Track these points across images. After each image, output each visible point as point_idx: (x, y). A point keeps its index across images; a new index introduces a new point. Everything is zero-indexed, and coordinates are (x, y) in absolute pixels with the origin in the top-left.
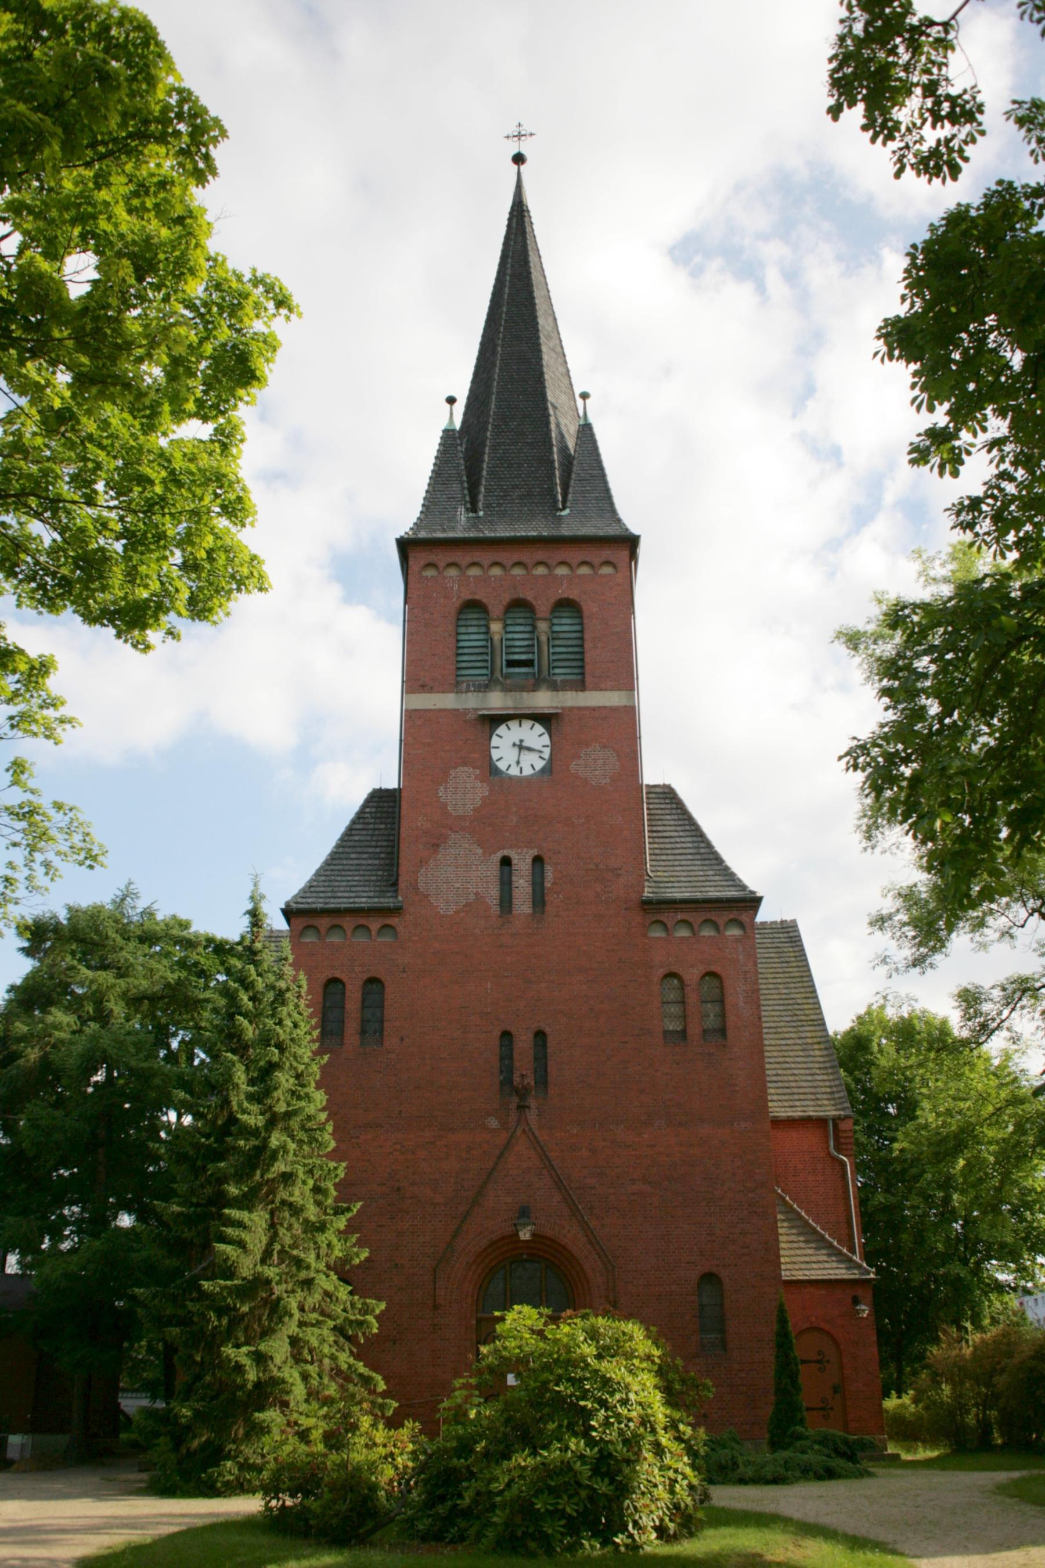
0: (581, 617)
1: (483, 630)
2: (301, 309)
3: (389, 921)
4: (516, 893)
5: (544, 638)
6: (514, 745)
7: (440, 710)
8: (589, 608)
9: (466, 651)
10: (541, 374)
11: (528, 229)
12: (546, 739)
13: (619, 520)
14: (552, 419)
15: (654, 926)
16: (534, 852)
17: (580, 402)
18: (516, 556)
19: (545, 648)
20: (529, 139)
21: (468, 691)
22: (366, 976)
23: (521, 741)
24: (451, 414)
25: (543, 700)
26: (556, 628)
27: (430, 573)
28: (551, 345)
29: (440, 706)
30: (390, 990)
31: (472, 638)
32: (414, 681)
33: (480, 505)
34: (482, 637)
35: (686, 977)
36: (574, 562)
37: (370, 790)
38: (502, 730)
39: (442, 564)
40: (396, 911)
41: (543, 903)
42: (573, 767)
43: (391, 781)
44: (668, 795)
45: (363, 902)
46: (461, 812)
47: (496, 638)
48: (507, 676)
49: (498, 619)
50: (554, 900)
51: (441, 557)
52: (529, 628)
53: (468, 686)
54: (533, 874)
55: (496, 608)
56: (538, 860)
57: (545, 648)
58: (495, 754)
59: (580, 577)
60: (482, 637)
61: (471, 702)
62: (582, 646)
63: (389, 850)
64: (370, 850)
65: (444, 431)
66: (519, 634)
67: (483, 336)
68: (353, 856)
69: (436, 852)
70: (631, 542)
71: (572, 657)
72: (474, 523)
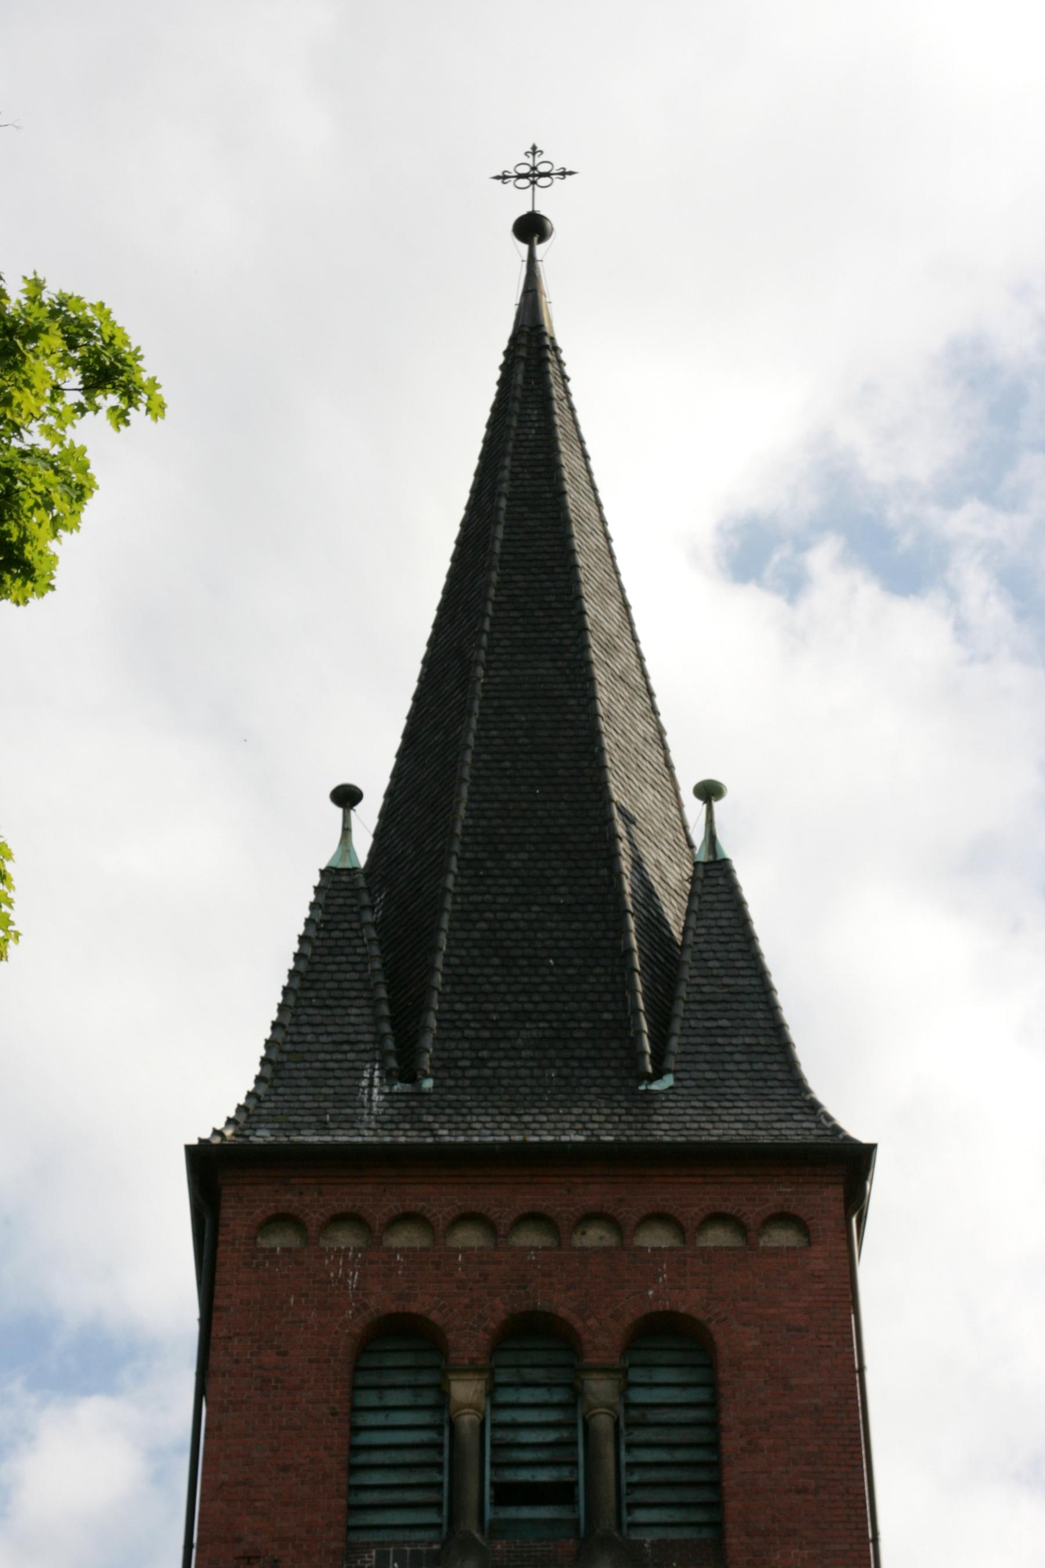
0: (711, 1366)
1: (429, 1398)
2: (165, 393)
5: (603, 1422)
9: (378, 1457)
10: (595, 735)
11: (556, 391)
13: (814, 1107)
14: (623, 846)
17: (694, 810)
19: (609, 1450)
20: (557, 181)
24: (346, 830)
26: (639, 1396)
27: (279, 1241)
28: (617, 666)
31: (397, 1422)
33: (426, 1062)
47: (467, 1420)
48: (498, 1530)
49: (473, 1369)
52: (558, 1396)
55: (468, 1341)
59: (709, 1255)
62: (714, 1446)
65: (325, 873)
66: (533, 1412)
67: (432, 643)
70: (852, 1163)
72: (409, 1108)
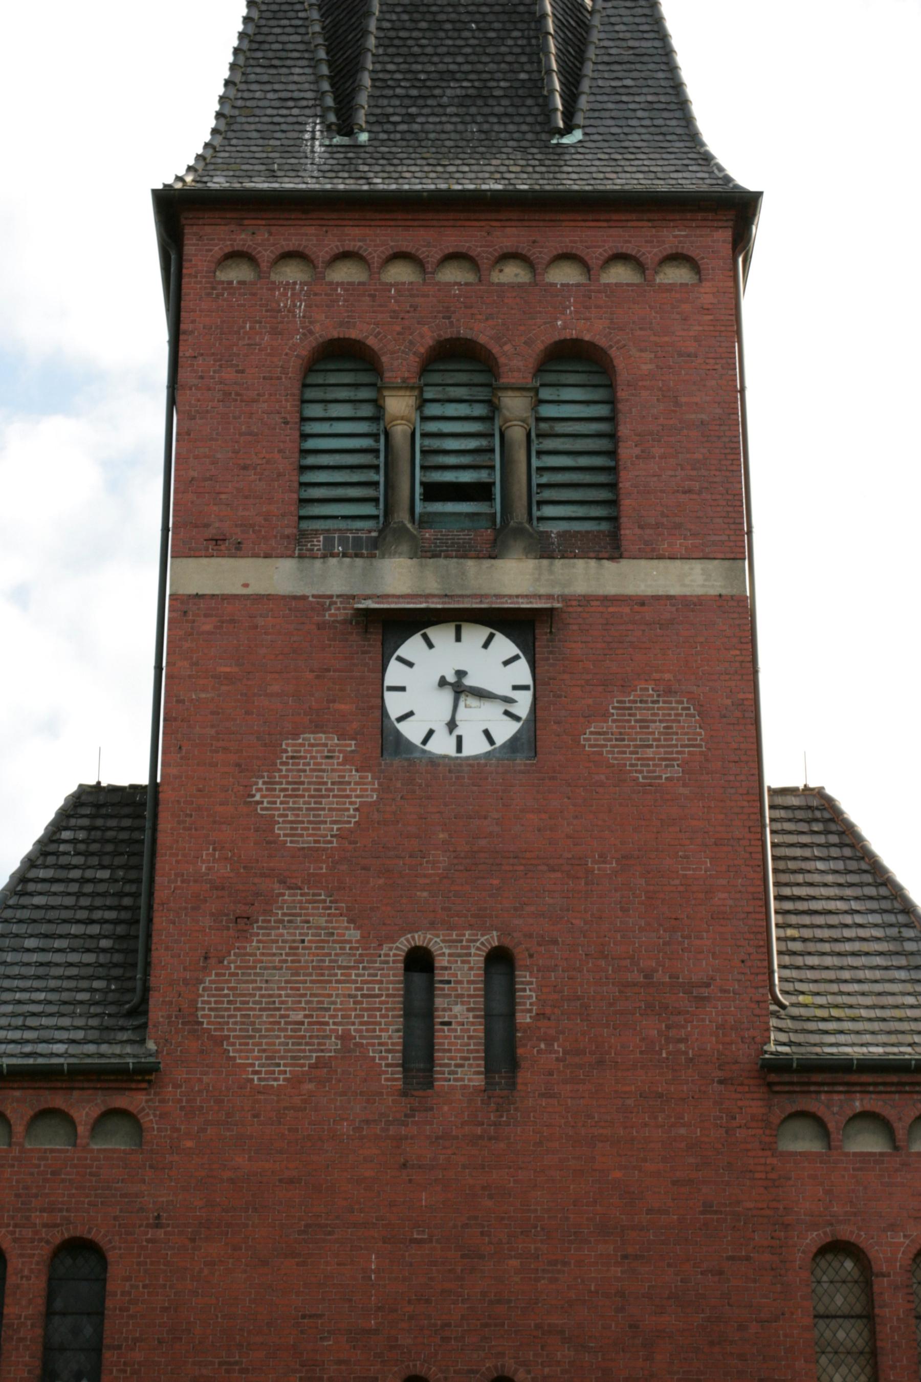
0: (611, 386)
1: (367, 411)
3: (120, 1101)
4: (444, 1038)
5: (517, 434)
6: (443, 682)
7: (258, 598)
8: (632, 362)
12: (522, 672)
13: (707, 159)
15: (798, 1126)
16: (493, 939)
18: (454, 238)
19: (520, 455)
21: (329, 554)
22: (58, 1236)
23: (461, 674)
25: (515, 578)
26: (547, 411)
27: (237, 273)
29: (257, 588)
30: (117, 1270)
31: (339, 428)
32: (190, 529)
33: (361, 117)
34: (362, 427)
35: (878, 1254)
36: (595, 255)
37: (72, 788)
38: (412, 647)
39: (266, 255)
40: (142, 1075)
41: (513, 1064)
42: (588, 739)
43: (130, 767)
44: (817, 813)
45: (58, 1052)
46: (307, 841)
47: (400, 431)
48: (426, 521)
50: (538, 1057)
51: (265, 239)
52: (479, 410)
53: (329, 542)
54: (488, 995)
55: (400, 363)
56: (500, 960)
57: (520, 455)
58: (395, 705)
60: (362, 427)
61: (336, 579)
62: (612, 454)
63: (120, 930)
64: (75, 929)
68: (30, 943)
69: (244, 935)
70: (736, 211)
71: (587, 478)
